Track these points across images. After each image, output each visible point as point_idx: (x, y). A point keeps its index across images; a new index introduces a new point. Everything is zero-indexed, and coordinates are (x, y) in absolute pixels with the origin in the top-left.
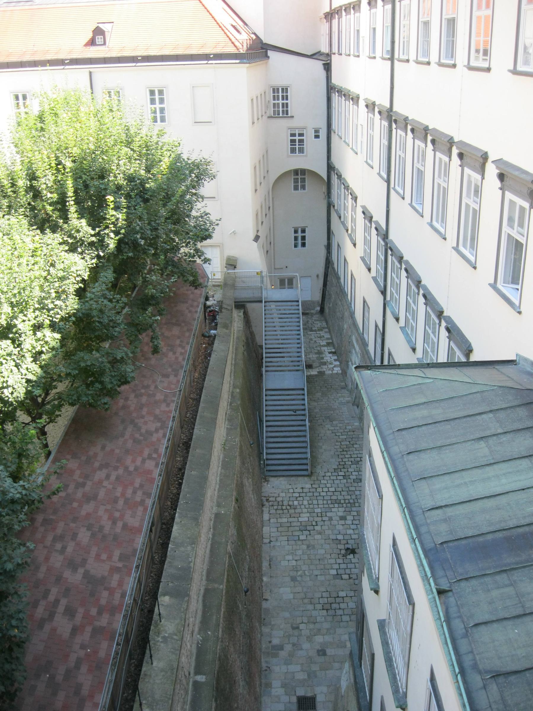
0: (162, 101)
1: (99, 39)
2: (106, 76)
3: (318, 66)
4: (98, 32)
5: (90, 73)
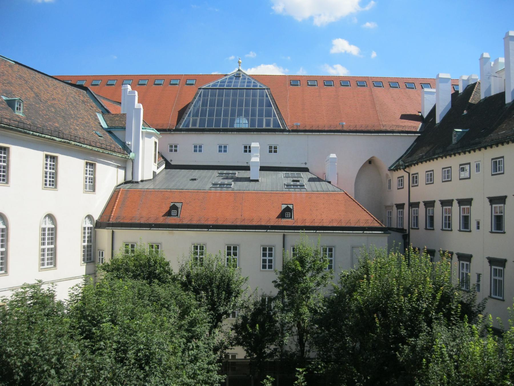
0: (270, 255)
1: (174, 212)
2: (296, 239)
3: (399, 235)
4: (174, 207)
5: (284, 236)
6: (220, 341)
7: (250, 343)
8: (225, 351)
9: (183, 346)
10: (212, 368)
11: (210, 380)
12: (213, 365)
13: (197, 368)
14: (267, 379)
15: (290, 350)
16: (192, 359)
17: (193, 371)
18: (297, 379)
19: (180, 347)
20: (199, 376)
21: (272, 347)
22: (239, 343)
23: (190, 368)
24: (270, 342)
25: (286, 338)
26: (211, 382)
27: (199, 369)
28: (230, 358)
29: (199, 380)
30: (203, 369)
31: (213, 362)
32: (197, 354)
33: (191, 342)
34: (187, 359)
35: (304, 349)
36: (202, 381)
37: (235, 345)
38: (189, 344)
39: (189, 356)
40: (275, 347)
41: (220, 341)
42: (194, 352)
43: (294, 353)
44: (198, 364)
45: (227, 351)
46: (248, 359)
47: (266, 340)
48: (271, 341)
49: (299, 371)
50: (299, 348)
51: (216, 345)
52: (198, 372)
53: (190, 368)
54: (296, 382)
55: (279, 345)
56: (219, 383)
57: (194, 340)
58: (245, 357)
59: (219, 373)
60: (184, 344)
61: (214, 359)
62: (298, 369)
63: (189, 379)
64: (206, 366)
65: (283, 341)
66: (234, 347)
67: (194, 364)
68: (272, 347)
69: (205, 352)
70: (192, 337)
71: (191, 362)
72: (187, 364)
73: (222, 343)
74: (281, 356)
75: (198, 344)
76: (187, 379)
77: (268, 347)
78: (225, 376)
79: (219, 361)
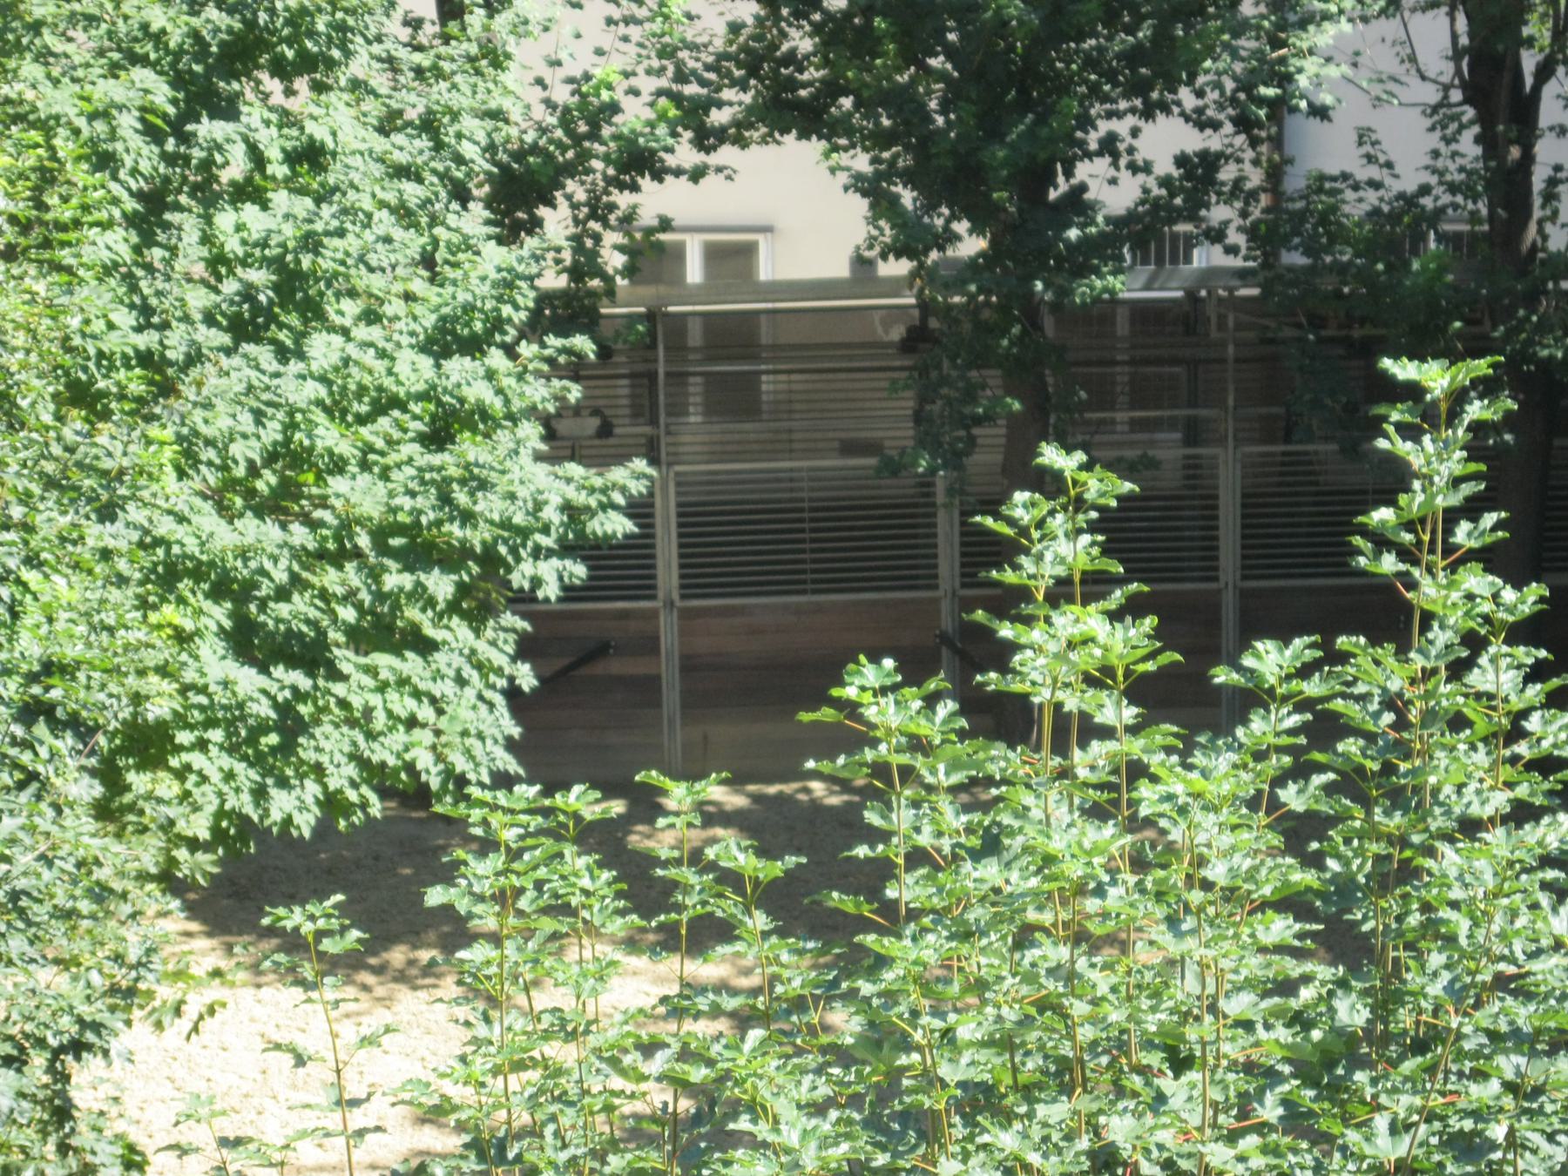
6: (562, 95)
7: (906, 105)
8: (623, 200)
9: (140, 155)
10: (480, 393)
11: (468, 517)
12: (496, 358)
13: (315, 390)
14: (1049, 483)
15: (1363, 173)
16: (248, 293)
17: (272, 432)
18: (1392, 480)
19: (104, 161)
20: (337, 484)
21: (1165, 141)
22: (788, 111)
23: (229, 396)
24: (1138, 88)
25: (1323, 37)
26: (477, 537)
27: (335, 410)
28: (694, 271)
29: (346, 526)
30: (386, 403)
31: (498, 324)
32: (311, 243)
33: (228, 110)
34: (198, 299)
35: (1528, 159)
36: (380, 535)
37: (735, 135)
38: (207, 129)
39: (219, 263)
40: (1193, 141)
41: (562, 95)
42: (280, 217)
43: (1409, 200)
44: (323, 349)
45: (652, 200)
46: (894, 286)
47: (1091, 62)
48: (1152, 78)
49: (1413, 391)
50: (1469, 147)
51: (519, 132)
52: (329, 437)
53: (229, 396)
54: (1382, 515)
55: (1244, 123)
56: (566, 549)
57: (273, 85)
58: (861, 263)
59: (560, 443)
60: (152, 133)
61: (507, 285)
62: (1403, 370)
63: (223, 509)
64: (414, 371)
65: (1285, 80)
66: (726, 154)
67: (283, 354)
68: (1165, 141)
69: (404, 214)
70: (241, 54)
71: (246, 326)
72: (195, 357)
73: (588, 113)
74: (1265, 238)
75: (318, 132)
76: (208, 519)
77: (1109, 146)
78: (633, 476)
79: (563, 312)
